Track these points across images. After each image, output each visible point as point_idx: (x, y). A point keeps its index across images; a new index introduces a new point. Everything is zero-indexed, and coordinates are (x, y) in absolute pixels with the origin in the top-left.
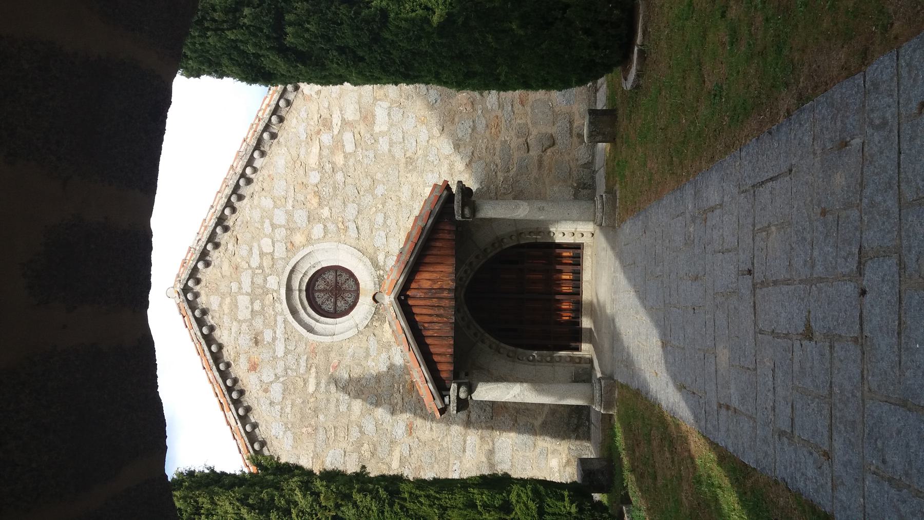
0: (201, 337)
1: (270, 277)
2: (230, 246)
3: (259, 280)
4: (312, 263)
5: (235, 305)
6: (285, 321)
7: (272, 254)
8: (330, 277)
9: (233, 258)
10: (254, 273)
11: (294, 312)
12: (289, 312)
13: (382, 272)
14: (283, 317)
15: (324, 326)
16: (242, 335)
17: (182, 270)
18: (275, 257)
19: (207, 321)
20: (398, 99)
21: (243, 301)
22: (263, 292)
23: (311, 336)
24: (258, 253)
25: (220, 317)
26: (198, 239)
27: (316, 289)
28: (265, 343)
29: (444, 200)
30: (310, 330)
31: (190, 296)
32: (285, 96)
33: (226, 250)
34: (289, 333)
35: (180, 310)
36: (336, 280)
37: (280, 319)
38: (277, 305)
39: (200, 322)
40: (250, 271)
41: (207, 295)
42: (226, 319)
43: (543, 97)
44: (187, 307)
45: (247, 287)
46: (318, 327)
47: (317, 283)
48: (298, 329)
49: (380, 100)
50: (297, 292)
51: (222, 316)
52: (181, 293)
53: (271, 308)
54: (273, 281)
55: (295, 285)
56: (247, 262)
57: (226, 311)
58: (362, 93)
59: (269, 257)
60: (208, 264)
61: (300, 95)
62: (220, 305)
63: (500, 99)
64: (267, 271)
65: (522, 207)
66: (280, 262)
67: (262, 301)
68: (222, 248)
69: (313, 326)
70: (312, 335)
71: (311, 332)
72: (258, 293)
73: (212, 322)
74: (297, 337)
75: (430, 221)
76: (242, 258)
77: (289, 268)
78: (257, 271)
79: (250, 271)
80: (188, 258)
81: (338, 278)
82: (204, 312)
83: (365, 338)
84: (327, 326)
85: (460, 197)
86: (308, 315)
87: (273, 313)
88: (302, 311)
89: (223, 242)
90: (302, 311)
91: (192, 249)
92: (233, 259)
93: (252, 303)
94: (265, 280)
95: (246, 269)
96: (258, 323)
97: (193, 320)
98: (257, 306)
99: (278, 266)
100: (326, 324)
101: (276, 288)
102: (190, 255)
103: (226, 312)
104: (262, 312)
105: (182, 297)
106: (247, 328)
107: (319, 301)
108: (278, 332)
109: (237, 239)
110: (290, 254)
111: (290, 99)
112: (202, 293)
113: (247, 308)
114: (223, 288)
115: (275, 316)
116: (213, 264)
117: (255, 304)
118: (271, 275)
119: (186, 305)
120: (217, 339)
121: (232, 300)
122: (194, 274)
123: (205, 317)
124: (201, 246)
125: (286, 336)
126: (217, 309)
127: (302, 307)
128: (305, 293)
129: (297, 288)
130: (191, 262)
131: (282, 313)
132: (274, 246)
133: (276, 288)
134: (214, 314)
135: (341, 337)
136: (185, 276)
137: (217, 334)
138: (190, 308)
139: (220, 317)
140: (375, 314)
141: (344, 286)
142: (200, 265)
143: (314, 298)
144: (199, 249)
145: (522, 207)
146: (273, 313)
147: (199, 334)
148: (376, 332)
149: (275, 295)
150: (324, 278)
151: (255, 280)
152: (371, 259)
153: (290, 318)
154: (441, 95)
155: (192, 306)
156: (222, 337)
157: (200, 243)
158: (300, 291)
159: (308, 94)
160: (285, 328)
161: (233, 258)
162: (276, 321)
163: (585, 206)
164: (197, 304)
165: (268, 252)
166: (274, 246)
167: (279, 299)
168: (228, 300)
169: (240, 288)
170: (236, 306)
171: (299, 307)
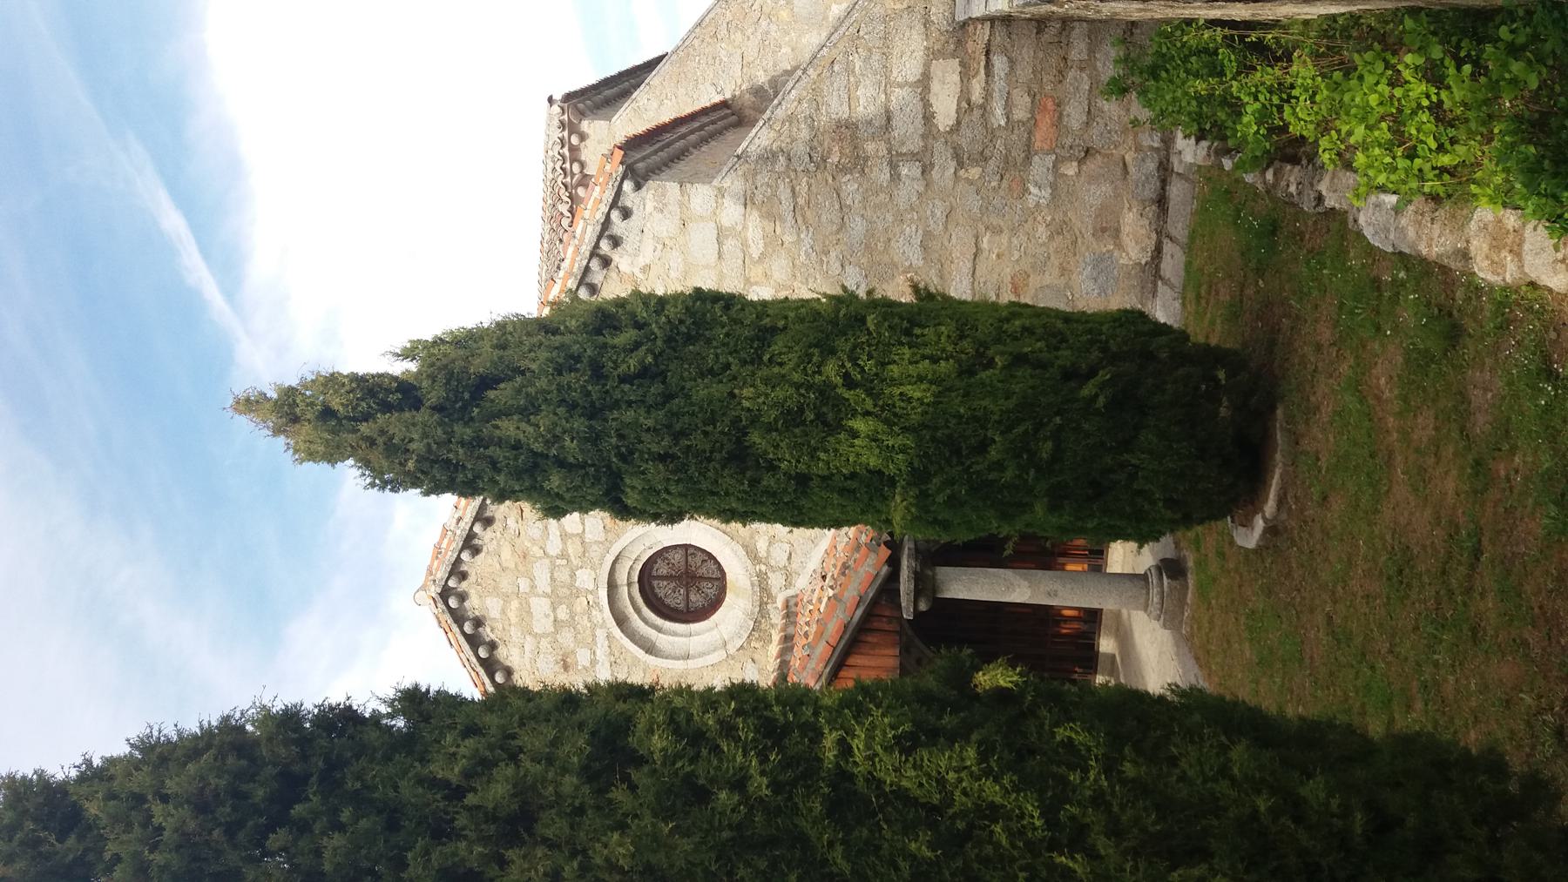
0: (477, 665)
1: (580, 571)
2: (511, 522)
3: (563, 576)
4: (647, 544)
5: (525, 612)
6: (609, 637)
7: (581, 536)
8: (677, 557)
9: (517, 541)
10: (553, 563)
11: (621, 621)
12: (614, 623)
13: (763, 568)
14: (605, 630)
15: (671, 638)
16: (542, 656)
17: (436, 563)
18: (587, 540)
19: (484, 635)
20: (789, 283)
21: (540, 606)
22: (571, 594)
23: (650, 659)
24: (558, 534)
25: (504, 629)
26: (457, 516)
27: (654, 573)
28: (580, 668)
29: (883, 580)
30: (650, 649)
31: (453, 603)
32: (588, 280)
33: (505, 528)
34: (617, 654)
35: (440, 622)
36: (687, 562)
37: (600, 634)
38: (594, 612)
39: (474, 641)
40: (547, 561)
41: (481, 597)
42: (515, 633)
43: (1056, 282)
44: (450, 621)
45: (543, 583)
46: (662, 641)
47: (656, 566)
48: (631, 649)
49: (756, 283)
50: (626, 588)
51: (507, 627)
52: (438, 599)
53: (585, 618)
54: (585, 577)
55: (622, 578)
56: (541, 548)
57: (514, 620)
58: (725, 271)
59: (577, 541)
60: (476, 551)
61: (613, 275)
62: (503, 612)
63: (976, 283)
64: (576, 562)
65: (1018, 590)
66: (595, 547)
67: (570, 607)
68: (497, 525)
69: (654, 639)
70: (653, 658)
71: (651, 654)
72: (564, 593)
73: (493, 636)
74: (629, 660)
75: (859, 612)
76: (533, 541)
77: (610, 559)
78: (559, 562)
79: (547, 561)
80: (444, 545)
81: (690, 558)
82: (478, 623)
83: (739, 665)
84: (676, 639)
85: (912, 586)
86: (646, 622)
87: (589, 625)
88: (634, 617)
89: (498, 516)
90: (634, 617)
91: (449, 533)
92: (518, 541)
93: (554, 610)
94: (573, 576)
95: (540, 558)
96: (566, 638)
97: (462, 640)
98: (562, 613)
99: (593, 554)
100: (675, 634)
101: (591, 587)
102: (446, 541)
103: (513, 622)
104: (572, 623)
105: (441, 606)
106: (549, 646)
107: (661, 593)
108: (598, 652)
109: (522, 511)
110: (610, 537)
111: (596, 282)
112: (473, 593)
113: (547, 616)
114: (505, 584)
115: (593, 629)
116: (485, 549)
117: (559, 611)
118: (581, 567)
119: (447, 617)
120: (502, 660)
121: (521, 603)
122: (457, 571)
123: (481, 629)
124: (464, 529)
125: (613, 659)
126: (498, 616)
127: (635, 642)
128: (637, 585)
129: (625, 581)
130: (450, 553)
131: (603, 625)
132: (583, 524)
133: (591, 587)
134: (495, 625)
135: (699, 663)
136: (441, 574)
137: (502, 653)
138: (456, 621)
139: (504, 629)
140: (753, 630)
141: (700, 571)
142: (465, 556)
143: (652, 588)
144: (461, 532)
145: (1018, 590)
146: (589, 625)
147: (474, 660)
148: (756, 657)
149: (590, 598)
150: (667, 558)
151: (555, 574)
152: (745, 547)
153: (617, 632)
154: (866, 276)
155: (458, 617)
156: (510, 658)
157: (462, 524)
158: (629, 584)
159: (628, 271)
160: (610, 647)
161: (517, 541)
162: (594, 636)
163: (1130, 594)
164: (465, 610)
165: (575, 532)
166: (583, 524)
167: (597, 604)
168: (515, 604)
169: (533, 587)
170: (529, 613)
171: (630, 610)
